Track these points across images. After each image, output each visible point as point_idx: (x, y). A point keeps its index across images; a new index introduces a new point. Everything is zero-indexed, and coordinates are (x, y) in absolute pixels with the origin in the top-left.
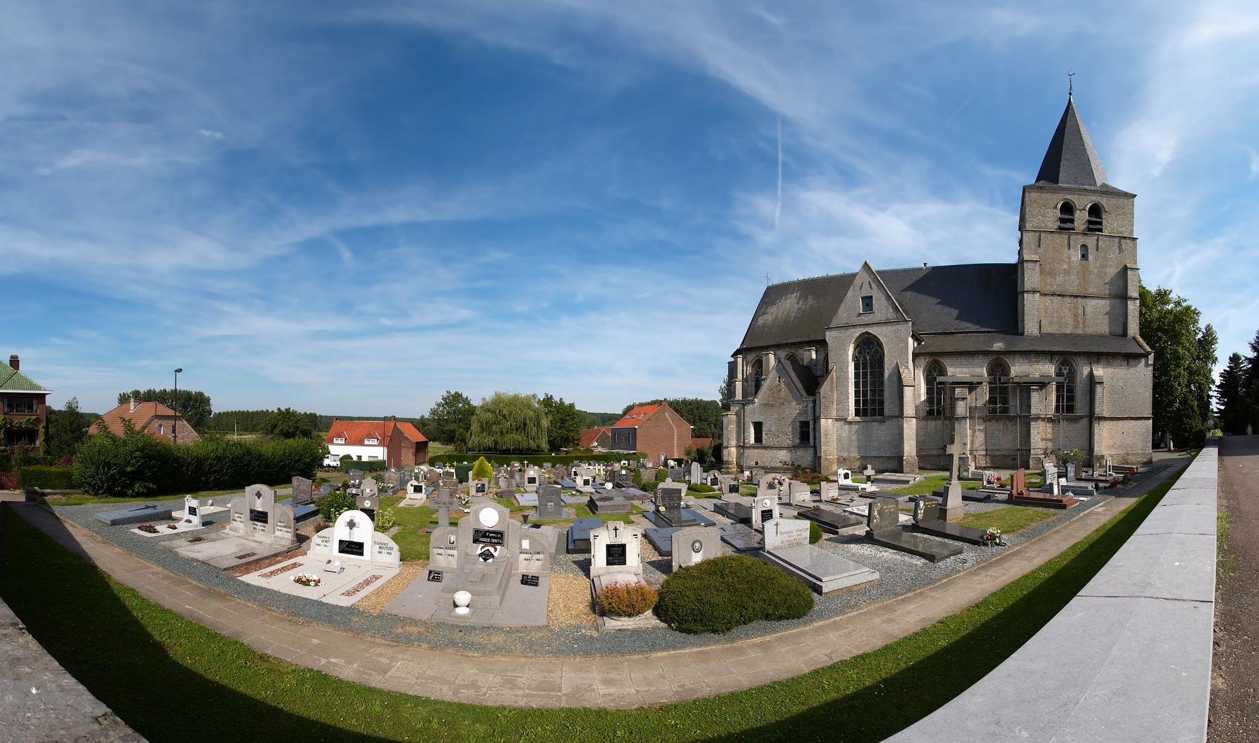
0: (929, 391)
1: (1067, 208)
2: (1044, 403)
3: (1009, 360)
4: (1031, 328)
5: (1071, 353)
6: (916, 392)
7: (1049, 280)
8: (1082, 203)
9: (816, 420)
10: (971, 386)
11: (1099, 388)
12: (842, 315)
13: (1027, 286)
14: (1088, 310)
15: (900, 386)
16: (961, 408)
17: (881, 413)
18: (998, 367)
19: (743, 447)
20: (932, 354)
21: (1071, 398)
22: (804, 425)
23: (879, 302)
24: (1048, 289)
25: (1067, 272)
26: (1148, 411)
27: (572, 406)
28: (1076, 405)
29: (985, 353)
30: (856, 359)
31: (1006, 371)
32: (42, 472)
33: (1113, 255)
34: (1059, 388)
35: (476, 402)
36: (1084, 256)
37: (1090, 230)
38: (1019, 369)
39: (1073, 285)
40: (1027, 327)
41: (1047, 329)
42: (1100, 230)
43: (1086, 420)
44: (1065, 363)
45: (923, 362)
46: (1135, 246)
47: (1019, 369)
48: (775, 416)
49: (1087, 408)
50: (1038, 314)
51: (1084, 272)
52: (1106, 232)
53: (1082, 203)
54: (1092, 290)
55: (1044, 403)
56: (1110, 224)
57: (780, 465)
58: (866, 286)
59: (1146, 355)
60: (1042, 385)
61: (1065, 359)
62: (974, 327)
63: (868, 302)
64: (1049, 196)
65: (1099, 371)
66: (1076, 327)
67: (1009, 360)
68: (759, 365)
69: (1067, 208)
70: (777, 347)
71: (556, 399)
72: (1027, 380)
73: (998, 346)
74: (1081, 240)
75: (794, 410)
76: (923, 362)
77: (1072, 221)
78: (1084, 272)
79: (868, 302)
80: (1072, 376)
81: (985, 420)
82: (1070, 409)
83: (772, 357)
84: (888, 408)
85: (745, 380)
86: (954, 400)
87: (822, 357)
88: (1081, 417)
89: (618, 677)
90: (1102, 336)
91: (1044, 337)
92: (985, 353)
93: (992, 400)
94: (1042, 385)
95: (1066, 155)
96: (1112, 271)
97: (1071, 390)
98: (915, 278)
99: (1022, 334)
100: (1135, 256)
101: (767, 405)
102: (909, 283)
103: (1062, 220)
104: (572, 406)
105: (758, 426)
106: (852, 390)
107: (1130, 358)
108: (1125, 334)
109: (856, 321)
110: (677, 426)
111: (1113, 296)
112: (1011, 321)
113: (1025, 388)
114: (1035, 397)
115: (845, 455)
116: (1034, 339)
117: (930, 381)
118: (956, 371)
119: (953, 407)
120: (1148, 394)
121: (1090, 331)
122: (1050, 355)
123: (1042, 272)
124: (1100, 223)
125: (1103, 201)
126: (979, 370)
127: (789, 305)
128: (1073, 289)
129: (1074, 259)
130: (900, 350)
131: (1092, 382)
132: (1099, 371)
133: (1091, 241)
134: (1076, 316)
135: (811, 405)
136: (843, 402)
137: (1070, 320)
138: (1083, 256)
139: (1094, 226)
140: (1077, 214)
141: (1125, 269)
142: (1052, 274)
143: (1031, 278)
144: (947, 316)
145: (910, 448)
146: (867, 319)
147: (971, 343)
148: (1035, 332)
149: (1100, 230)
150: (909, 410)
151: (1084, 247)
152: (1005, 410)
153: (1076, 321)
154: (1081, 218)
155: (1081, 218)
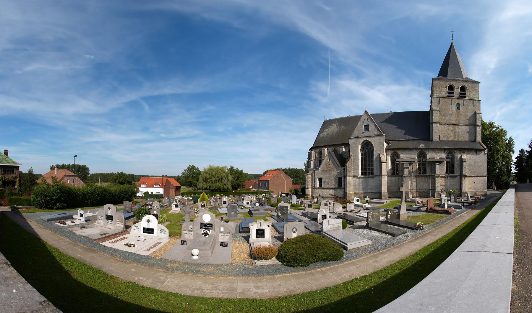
0: (393, 165)
1: (451, 88)
2: (441, 170)
3: (426, 152)
4: (435, 138)
5: (452, 149)
6: (387, 165)
7: (443, 118)
8: (457, 86)
9: (345, 177)
10: (411, 163)
11: (464, 163)
12: (356, 133)
13: (434, 121)
14: (460, 131)
15: (380, 162)
16: (406, 172)
17: (372, 174)
18: (422, 155)
19: (314, 188)
20: (394, 149)
21: (453, 168)
22: (340, 179)
23: (372, 127)
24: (443, 122)
25: (451, 115)
26: (485, 173)
27: (242, 171)
28: (455, 171)
29: (416, 149)
30: (362, 151)
31: (425, 156)
32: (18, 199)
33: (470, 107)
34: (448, 163)
35: (201, 169)
36: (458, 108)
37: (460, 97)
38: (431, 156)
39: (453, 120)
40: (434, 138)
41: (442, 139)
42: (465, 97)
43: (459, 177)
44: (450, 153)
45: (390, 152)
46: (480, 104)
47: (431, 156)
48: (328, 175)
49: (459, 172)
50: (438, 132)
51: (458, 115)
52: (467, 98)
53: (457, 86)
54: (461, 122)
55: (441, 170)
56: (469, 94)
57: (329, 196)
58: (366, 121)
59: (484, 150)
60: (440, 162)
61: (450, 151)
62: (411, 138)
63: (367, 127)
64: (443, 82)
65: (464, 156)
66: (455, 138)
67: (426, 152)
68: (321, 154)
69: (451, 88)
70: (328, 146)
71: (235, 168)
72: (434, 160)
73: (422, 146)
74: (457, 101)
75: (335, 173)
76: (390, 152)
77: (453, 93)
78: (458, 115)
79: (367, 127)
80: (453, 158)
81: (416, 177)
82: (452, 172)
83: (326, 150)
84: (375, 172)
85: (315, 160)
86: (403, 169)
87: (347, 151)
88: (457, 176)
89: (261, 285)
90: (466, 142)
91: (441, 142)
92: (416, 149)
93: (419, 169)
94: (440, 162)
95: (451, 65)
96: (470, 114)
97: (452, 164)
98: (387, 117)
99: (432, 141)
100: (480, 108)
101: (324, 171)
102: (384, 119)
103: (449, 93)
104: (242, 171)
105: (320, 180)
106: (360, 164)
107: (478, 151)
108: (475, 141)
109: (362, 135)
110: (286, 180)
111: (470, 125)
112: (427, 135)
113: (433, 163)
114: (437, 167)
115: (357, 191)
116: (437, 143)
117: (393, 161)
118: (404, 156)
119: (403, 172)
120: (485, 166)
121: (461, 139)
122: (444, 150)
123: (440, 115)
124: (465, 94)
125: (466, 85)
126: (414, 156)
127: (334, 129)
128: (453, 122)
129: (454, 109)
130: (380, 147)
131: (462, 161)
132: (464, 156)
133: (461, 102)
134: (454, 133)
135: (343, 171)
136: (356, 169)
137: (452, 135)
138: (458, 108)
139: (462, 95)
140: (455, 90)
141: (476, 113)
142: (445, 115)
143: (436, 117)
144: (400, 133)
145: (384, 189)
146: (366, 134)
147: (410, 145)
148: (438, 140)
149: (465, 97)
150: (384, 173)
151: (458, 104)
152: (425, 173)
153: (455, 135)
154: (457, 92)
155: (457, 92)
